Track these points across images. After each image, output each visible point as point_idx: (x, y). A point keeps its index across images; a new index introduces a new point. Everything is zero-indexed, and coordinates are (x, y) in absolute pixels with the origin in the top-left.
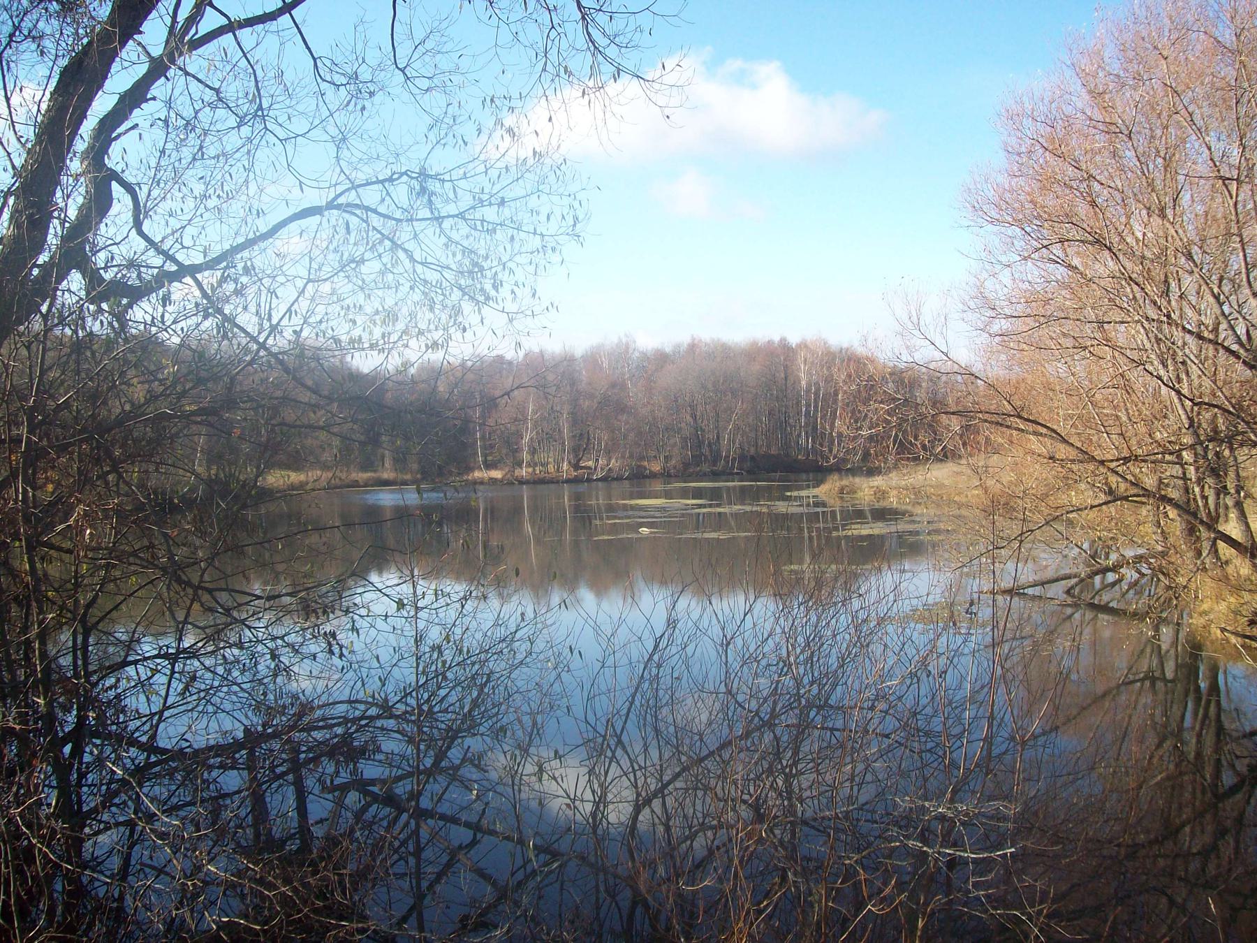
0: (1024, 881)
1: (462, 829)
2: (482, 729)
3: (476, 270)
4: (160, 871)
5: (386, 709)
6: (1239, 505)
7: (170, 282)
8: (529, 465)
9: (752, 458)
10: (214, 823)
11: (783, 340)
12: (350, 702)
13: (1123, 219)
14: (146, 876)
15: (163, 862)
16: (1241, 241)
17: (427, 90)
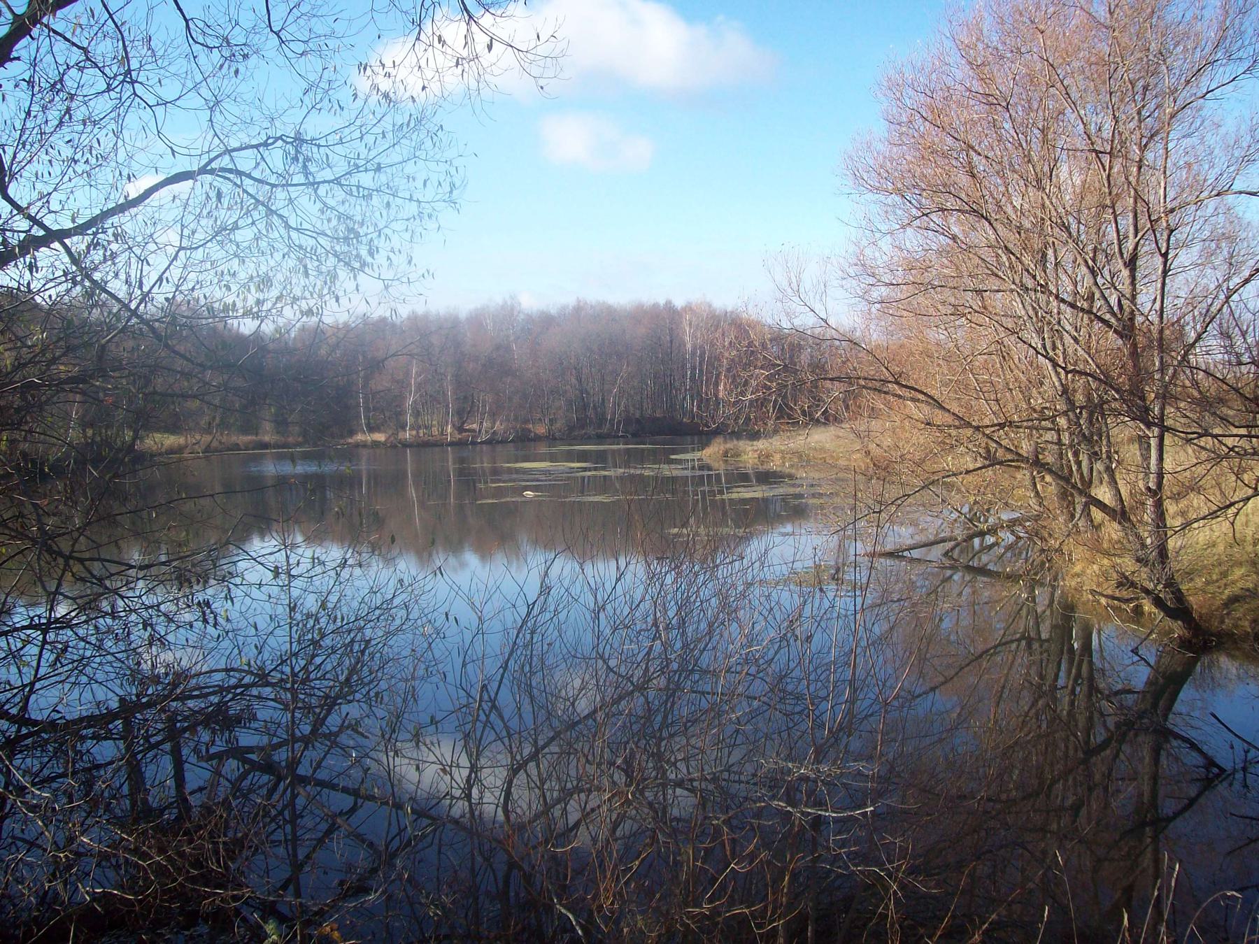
0: (884, 838)
1: (340, 795)
2: (358, 696)
3: (351, 236)
4: (32, 845)
5: (263, 678)
6: (1110, 472)
7: (37, 249)
8: (412, 428)
9: (638, 421)
10: (87, 795)
11: (668, 303)
12: (227, 670)
13: (1002, 189)
14: (18, 850)
15: (34, 834)
16: (1114, 212)
17: (302, 55)
